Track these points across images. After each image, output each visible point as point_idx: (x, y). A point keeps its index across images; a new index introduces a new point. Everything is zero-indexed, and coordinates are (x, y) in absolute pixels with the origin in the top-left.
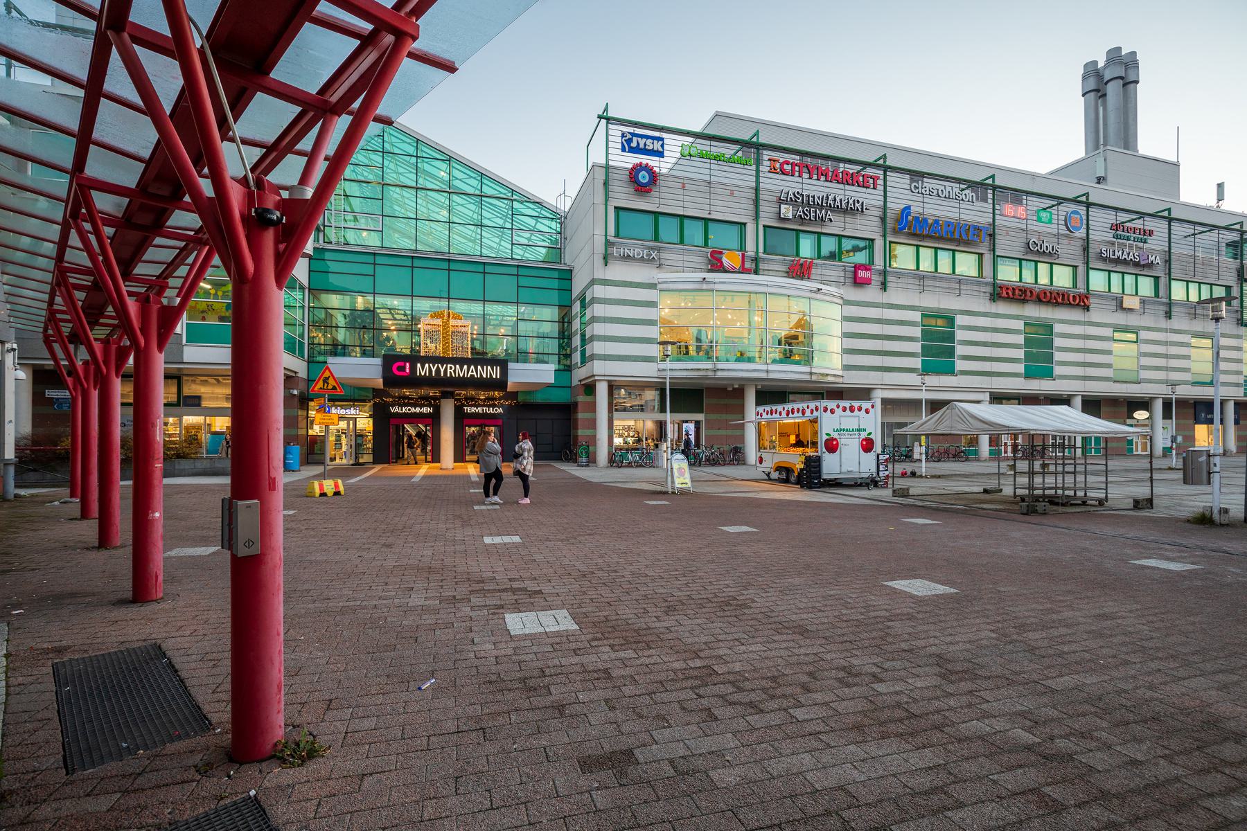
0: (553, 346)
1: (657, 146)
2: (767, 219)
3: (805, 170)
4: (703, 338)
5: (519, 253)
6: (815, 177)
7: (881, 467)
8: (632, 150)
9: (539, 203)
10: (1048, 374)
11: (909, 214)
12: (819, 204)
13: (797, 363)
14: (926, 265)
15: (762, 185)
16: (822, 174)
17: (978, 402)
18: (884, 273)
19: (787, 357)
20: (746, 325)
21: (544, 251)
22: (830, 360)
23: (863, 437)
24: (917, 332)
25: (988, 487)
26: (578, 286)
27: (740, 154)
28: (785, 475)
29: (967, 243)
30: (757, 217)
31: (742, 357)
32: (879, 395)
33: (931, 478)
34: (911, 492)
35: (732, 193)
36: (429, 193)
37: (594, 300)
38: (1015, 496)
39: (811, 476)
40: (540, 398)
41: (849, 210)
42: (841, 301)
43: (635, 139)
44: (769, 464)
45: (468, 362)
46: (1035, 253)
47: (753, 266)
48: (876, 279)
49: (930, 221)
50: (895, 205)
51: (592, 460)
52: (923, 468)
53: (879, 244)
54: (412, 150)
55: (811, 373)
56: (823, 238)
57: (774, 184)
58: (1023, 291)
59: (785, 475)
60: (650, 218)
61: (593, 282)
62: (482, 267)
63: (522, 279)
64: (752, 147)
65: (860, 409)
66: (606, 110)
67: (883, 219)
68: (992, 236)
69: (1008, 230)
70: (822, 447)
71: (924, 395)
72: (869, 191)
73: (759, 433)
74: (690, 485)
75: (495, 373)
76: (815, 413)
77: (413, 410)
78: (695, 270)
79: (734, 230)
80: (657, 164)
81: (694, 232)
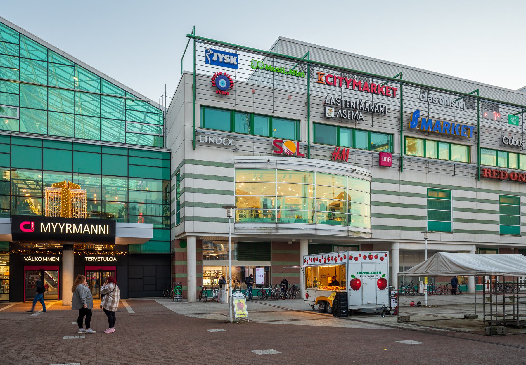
0: (159, 210)
1: (233, 60)
2: (316, 117)
3: (343, 82)
4: (269, 204)
5: (132, 139)
6: (351, 87)
7: (392, 300)
8: (214, 62)
9: (146, 102)
10: (517, 232)
11: (418, 116)
12: (354, 106)
13: (339, 224)
14: (431, 153)
15: (312, 93)
16: (356, 85)
17: (468, 252)
18: (401, 159)
19: (332, 219)
20: (302, 195)
21: (152, 138)
22: (362, 223)
23: (379, 278)
24: (424, 201)
25: (468, 314)
26: (175, 164)
27: (297, 69)
28: (323, 308)
29: (460, 138)
30: (308, 116)
31: (299, 220)
32: (397, 247)
33: (433, 308)
34: (412, 318)
35: (290, 98)
36: (62, 91)
37: (185, 175)
38: (485, 321)
39: (340, 307)
40: (145, 249)
41: (377, 113)
42: (370, 179)
43: (216, 54)
44: (312, 299)
45: (89, 221)
46: (507, 146)
47: (306, 152)
48: (395, 163)
49: (433, 122)
50: (409, 109)
51: (184, 296)
52: (426, 300)
53: (397, 137)
54: (44, 56)
55: (348, 231)
56: (357, 133)
57: (321, 92)
58: (499, 173)
59: (323, 308)
60: (228, 115)
61: (184, 162)
62: (101, 149)
63: (133, 159)
64: (306, 63)
65: (376, 257)
66: (193, 31)
67: (400, 120)
68: (477, 133)
69: (488, 129)
70: (348, 286)
71: (427, 247)
72: (389, 98)
73: (306, 276)
74: (247, 316)
75: (105, 230)
76: (344, 261)
77: (43, 259)
78: (262, 154)
79: (292, 124)
80: (233, 74)
81: (261, 125)
